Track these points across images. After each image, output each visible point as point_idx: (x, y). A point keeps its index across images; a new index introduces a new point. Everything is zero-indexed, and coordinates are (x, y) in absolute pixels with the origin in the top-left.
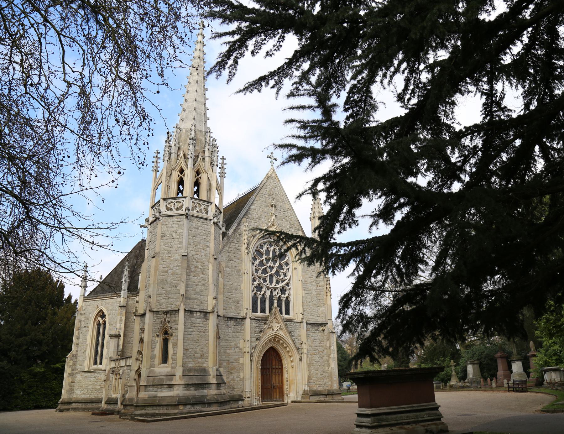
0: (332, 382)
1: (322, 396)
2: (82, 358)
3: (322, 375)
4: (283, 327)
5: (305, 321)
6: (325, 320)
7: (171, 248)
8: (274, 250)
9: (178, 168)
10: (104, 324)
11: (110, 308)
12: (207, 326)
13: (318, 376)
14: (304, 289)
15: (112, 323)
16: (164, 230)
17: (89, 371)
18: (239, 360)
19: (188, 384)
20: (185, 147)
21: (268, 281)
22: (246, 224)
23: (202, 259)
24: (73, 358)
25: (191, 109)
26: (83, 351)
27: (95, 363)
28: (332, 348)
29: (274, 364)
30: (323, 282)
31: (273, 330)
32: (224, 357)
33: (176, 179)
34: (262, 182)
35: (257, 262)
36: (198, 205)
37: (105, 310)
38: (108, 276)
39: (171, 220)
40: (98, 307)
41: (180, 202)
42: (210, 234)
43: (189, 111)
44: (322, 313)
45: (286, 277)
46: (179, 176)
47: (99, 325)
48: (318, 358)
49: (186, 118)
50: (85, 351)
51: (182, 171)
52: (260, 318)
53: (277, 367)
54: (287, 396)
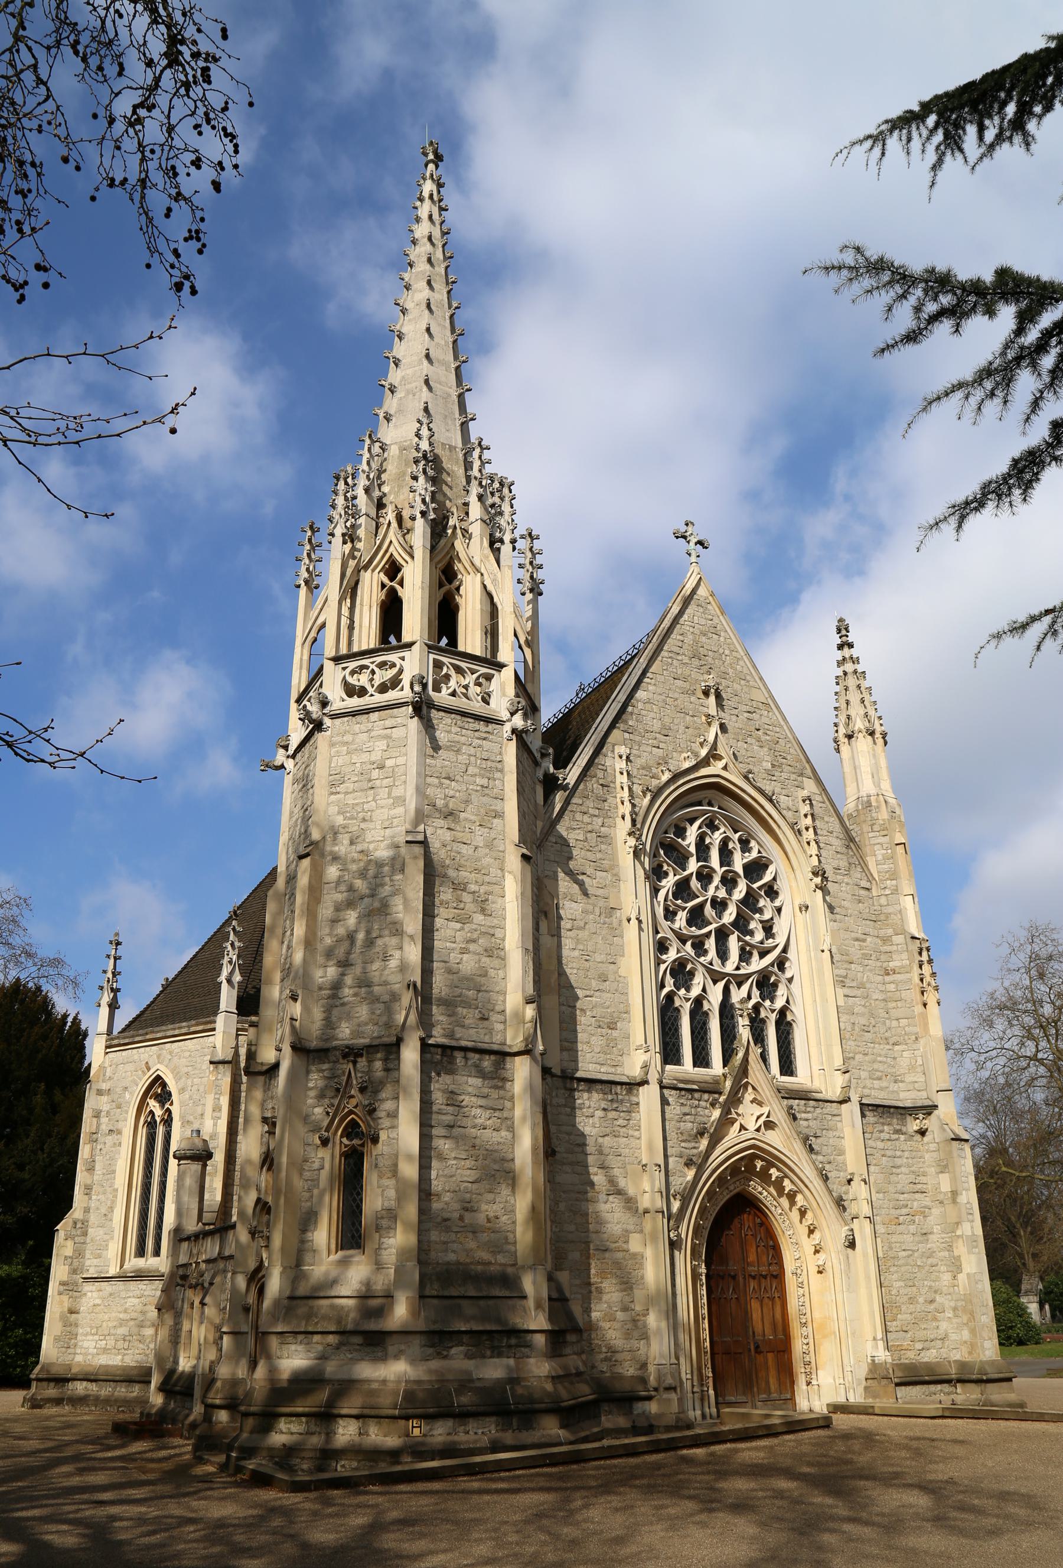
0: (973, 1331)
1: (939, 1387)
2: (101, 1231)
3: (932, 1302)
4: (780, 1116)
5: (855, 1098)
6: (924, 1094)
7: (364, 820)
8: (725, 842)
9: (380, 561)
10: (168, 1121)
11: (186, 1070)
12: (508, 1104)
13: (919, 1307)
14: (841, 982)
15: (191, 1118)
16: (341, 762)
17: (123, 1277)
18: (627, 1242)
19: (441, 1334)
20: (402, 497)
21: (712, 954)
22: (623, 750)
23: (478, 859)
24: (74, 1232)
25: (414, 385)
26: (103, 1210)
27: (141, 1252)
28: (963, 1199)
29: (752, 1257)
30: (905, 956)
31: (742, 1128)
32: (572, 1228)
33: (374, 598)
34: (655, 631)
35: (669, 883)
36: (452, 672)
37: (170, 1076)
38: (180, 972)
39: (363, 728)
40: (149, 1069)
41: (393, 665)
42: (501, 771)
43: (408, 392)
44: (912, 1068)
45: (773, 936)
46: (383, 586)
47: (151, 1125)
48: (909, 1238)
49: (400, 411)
50: (111, 1209)
51: (393, 570)
52: (693, 1082)
53: (764, 1270)
54: (808, 1383)
